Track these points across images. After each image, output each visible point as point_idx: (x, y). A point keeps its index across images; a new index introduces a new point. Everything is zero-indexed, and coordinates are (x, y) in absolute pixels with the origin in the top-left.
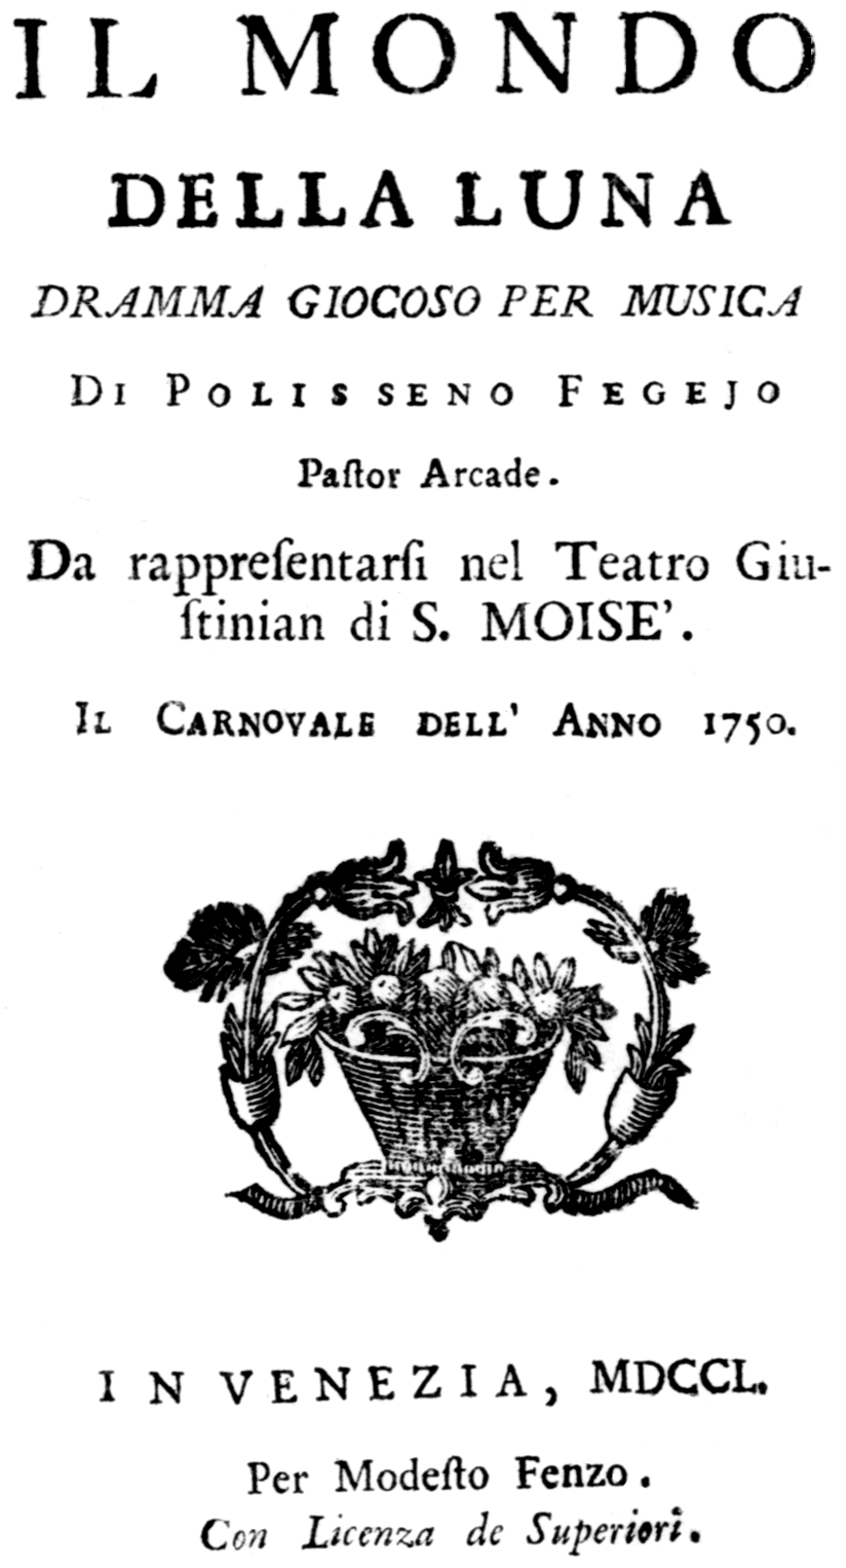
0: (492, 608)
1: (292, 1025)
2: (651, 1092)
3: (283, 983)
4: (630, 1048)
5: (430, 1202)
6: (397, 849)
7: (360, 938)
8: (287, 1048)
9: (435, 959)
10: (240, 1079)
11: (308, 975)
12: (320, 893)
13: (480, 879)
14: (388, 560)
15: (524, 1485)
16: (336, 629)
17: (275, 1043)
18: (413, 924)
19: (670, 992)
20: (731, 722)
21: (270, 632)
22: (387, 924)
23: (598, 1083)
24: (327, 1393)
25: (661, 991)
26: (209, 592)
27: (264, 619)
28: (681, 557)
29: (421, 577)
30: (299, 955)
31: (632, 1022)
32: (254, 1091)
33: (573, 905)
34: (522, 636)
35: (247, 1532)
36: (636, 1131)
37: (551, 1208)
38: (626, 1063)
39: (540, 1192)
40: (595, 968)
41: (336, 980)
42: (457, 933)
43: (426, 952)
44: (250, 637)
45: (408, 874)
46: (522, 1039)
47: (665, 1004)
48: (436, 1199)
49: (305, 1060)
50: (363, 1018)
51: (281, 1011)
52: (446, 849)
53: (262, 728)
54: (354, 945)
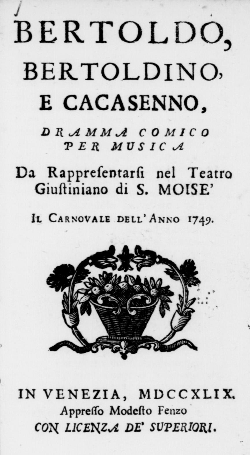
0: (161, 186)
1: (82, 298)
2: (183, 317)
3: (78, 286)
4: (178, 305)
5: (122, 348)
6: (112, 249)
7: (102, 274)
8: (81, 304)
9: (123, 280)
10: (68, 313)
11: (87, 284)
12: (90, 261)
13: (136, 257)
14: (132, 172)
15: (160, 414)
16: (112, 190)
17: (77, 303)
18: (117, 270)
19: (189, 288)
20: (195, 219)
21: (85, 192)
22: (109, 270)
23: (169, 314)
24: (71, 397)
25: (186, 287)
26: (78, 181)
27: (83, 188)
28: (223, 172)
29: (142, 177)
30: (84, 278)
31: (178, 297)
32: (72, 318)
33: (161, 265)
34: (169, 194)
35: (41, 431)
36: (74, 298)
37: (156, 350)
38: (177, 309)
39: (153, 345)
40: (167, 281)
41: (94, 285)
42: (129, 272)
43: (120, 277)
44: (78, 193)
45: (115, 255)
46: (147, 302)
47: (187, 291)
48: (123, 348)
49: (86, 308)
50: (101, 296)
51: (79, 294)
52: (126, 249)
53: (183, 106)
54: (100, 275)
